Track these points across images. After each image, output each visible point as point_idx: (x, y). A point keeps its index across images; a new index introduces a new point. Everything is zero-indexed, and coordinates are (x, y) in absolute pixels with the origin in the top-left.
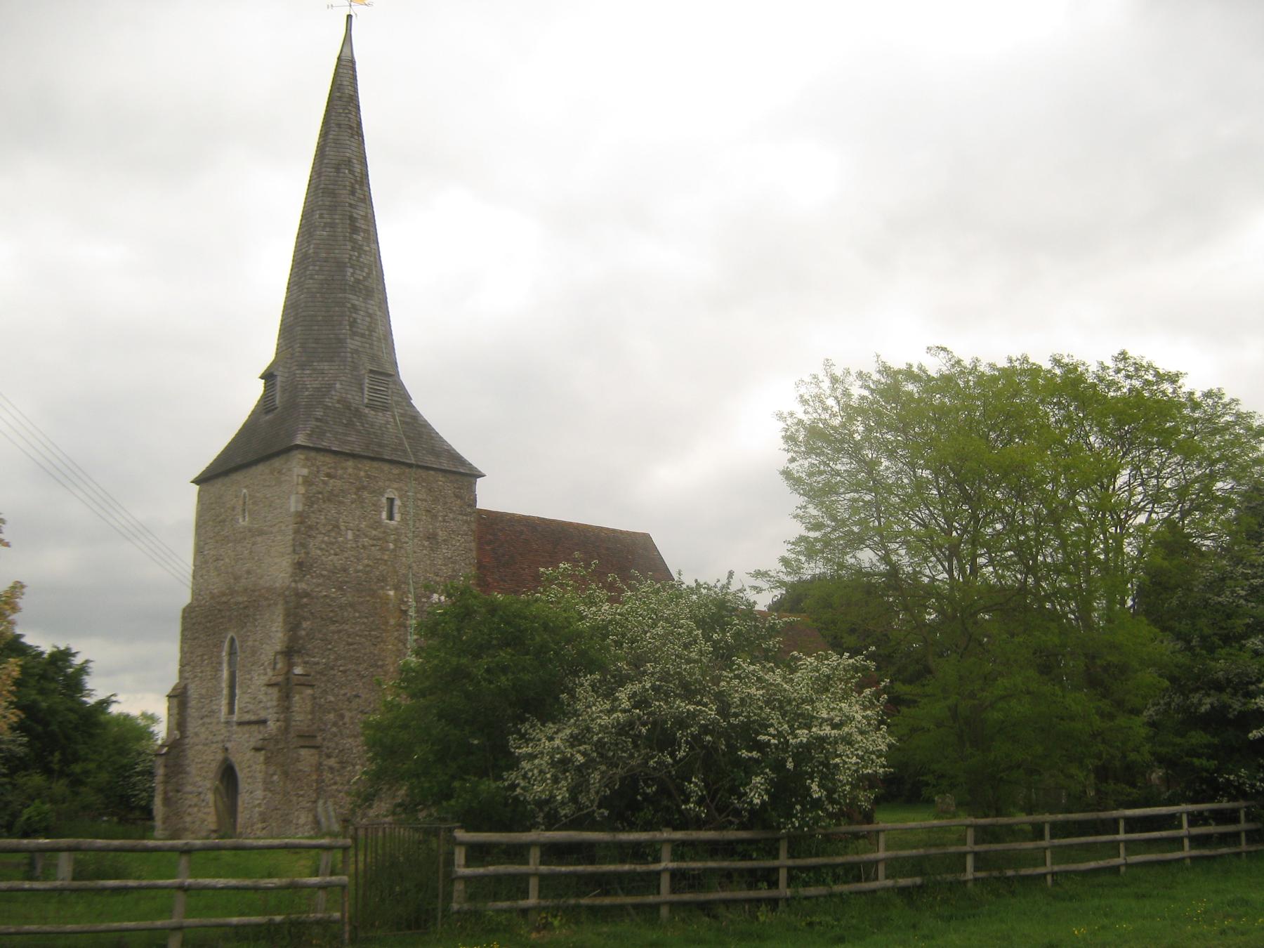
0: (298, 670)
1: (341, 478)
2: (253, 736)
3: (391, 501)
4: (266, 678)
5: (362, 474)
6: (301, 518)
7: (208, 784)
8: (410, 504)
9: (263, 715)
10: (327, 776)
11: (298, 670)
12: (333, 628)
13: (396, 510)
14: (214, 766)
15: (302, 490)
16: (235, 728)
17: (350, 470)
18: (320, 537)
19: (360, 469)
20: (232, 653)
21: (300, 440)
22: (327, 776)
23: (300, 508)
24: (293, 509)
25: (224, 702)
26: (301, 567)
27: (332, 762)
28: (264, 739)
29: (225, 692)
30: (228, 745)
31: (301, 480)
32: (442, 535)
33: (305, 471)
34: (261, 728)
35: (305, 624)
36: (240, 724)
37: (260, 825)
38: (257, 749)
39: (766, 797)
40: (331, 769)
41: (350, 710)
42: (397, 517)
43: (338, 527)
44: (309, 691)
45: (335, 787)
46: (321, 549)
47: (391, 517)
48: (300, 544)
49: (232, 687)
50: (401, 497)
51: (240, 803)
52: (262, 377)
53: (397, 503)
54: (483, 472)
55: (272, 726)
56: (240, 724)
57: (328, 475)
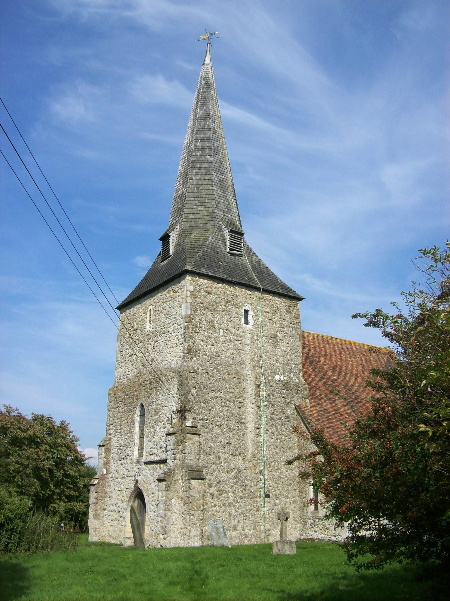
0: (189, 423)
1: (215, 294)
2: (102, 515)
3: (246, 312)
4: (166, 430)
5: (228, 292)
6: (189, 319)
7: (215, 543)
8: (259, 314)
9: (163, 456)
10: (209, 499)
11: (189, 423)
12: (211, 395)
13: (250, 318)
14: (129, 493)
15: (190, 300)
16: (144, 466)
17: (220, 290)
18: (202, 332)
19: (227, 290)
20: (142, 415)
21: (188, 268)
22: (209, 499)
23: (189, 312)
24: (184, 314)
25: (136, 448)
26: (190, 352)
27: (213, 490)
28: (165, 473)
29: (137, 441)
30: (139, 478)
31: (189, 293)
32: (280, 336)
33: (192, 288)
34: (162, 466)
35: (194, 391)
36: (146, 463)
37: (162, 536)
38: (160, 480)
39: (385, 517)
40: (212, 494)
41: (224, 453)
42: (251, 322)
43: (214, 326)
44: (196, 438)
45: (214, 509)
46: (203, 341)
47: (247, 322)
48: (187, 337)
49: (142, 437)
50: (253, 310)
51: (147, 519)
52: (160, 240)
53: (251, 313)
54: (303, 297)
55: (170, 463)
56: (146, 463)
57: (207, 292)
